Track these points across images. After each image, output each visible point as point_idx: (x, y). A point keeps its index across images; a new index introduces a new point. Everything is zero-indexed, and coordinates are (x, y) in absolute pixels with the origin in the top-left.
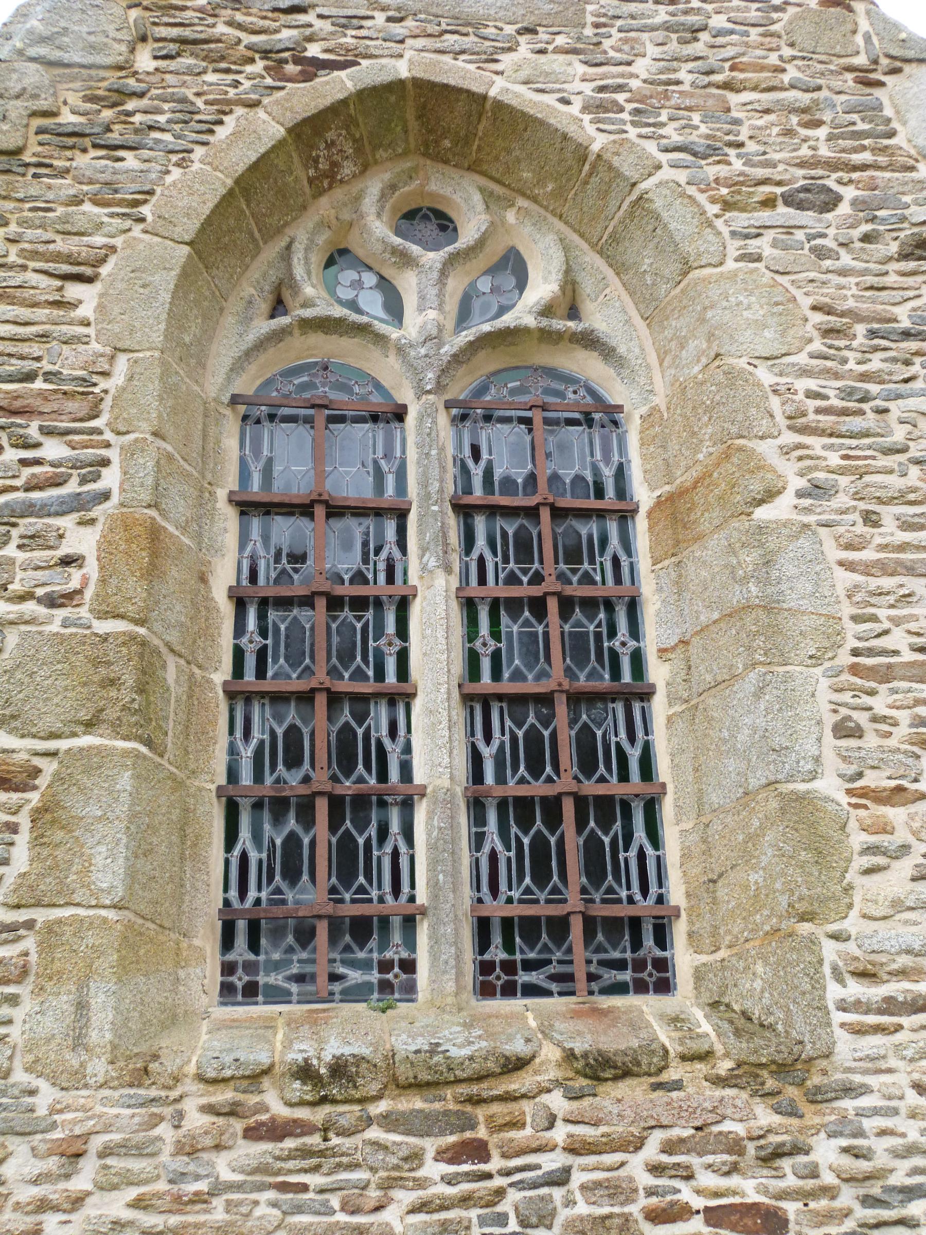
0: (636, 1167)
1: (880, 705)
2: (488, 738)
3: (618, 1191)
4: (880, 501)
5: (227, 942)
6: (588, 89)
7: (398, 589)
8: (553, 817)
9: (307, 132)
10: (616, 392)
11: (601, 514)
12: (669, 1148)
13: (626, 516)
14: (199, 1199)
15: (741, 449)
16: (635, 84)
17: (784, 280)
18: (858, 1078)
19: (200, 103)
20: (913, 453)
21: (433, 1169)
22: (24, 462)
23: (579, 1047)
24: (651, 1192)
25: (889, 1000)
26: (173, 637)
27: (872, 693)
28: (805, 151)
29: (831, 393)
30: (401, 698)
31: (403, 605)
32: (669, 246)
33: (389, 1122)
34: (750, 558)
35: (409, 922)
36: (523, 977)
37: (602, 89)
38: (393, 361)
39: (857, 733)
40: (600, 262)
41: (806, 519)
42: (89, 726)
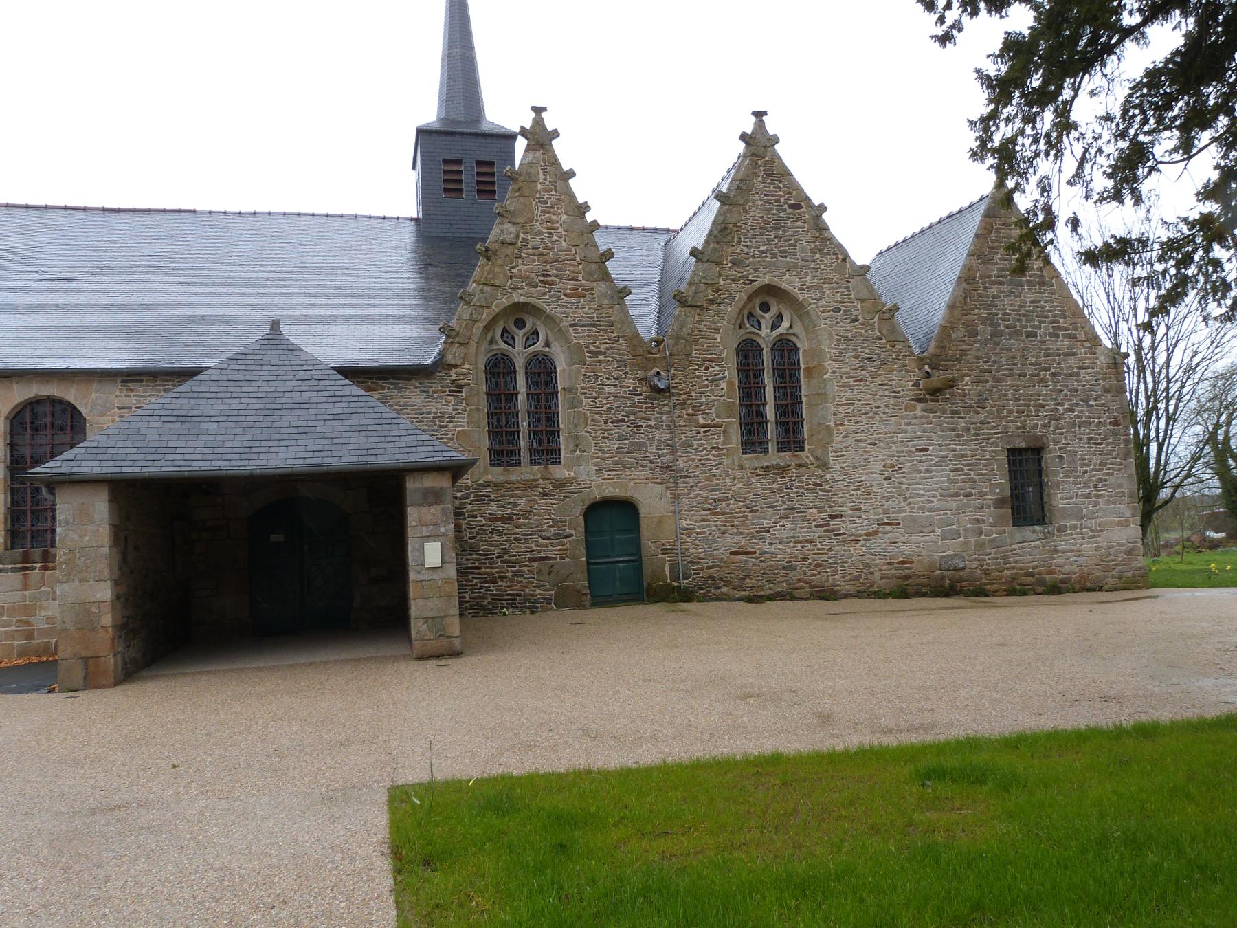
10: (799, 345)
32: (811, 321)
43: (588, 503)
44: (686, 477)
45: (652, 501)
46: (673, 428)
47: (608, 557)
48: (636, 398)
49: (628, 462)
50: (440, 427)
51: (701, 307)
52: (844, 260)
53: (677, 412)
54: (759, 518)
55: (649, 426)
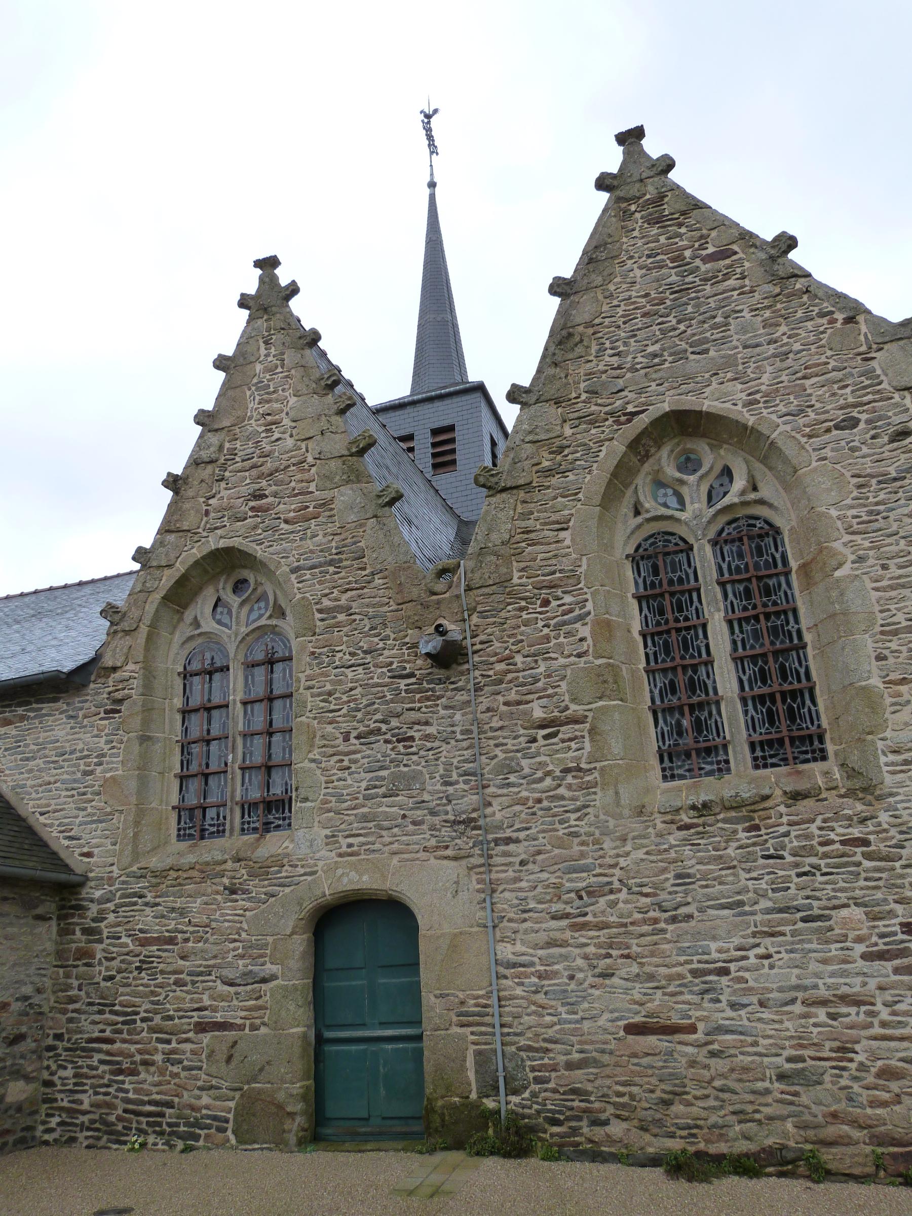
0: (813, 828)
1: (894, 646)
2: (744, 673)
3: (809, 837)
4: (888, 559)
5: (662, 761)
6: (743, 396)
7: (701, 621)
8: (774, 702)
9: (634, 445)
10: (778, 522)
11: (777, 575)
12: (825, 821)
13: (787, 574)
14: (665, 850)
15: (826, 548)
16: (763, 388)
17: (838, 466)
18: (895, 790)
19: (591, 444)
20: (901, 534)
21: (742, 835)
22: (559, 606)
23: (788, 789)
24: (819, 836)
25: (905, 760)
26: (622, 659)
27: (890, 641)
28: (842, 402)
29: (863, 514)
30: (709, 663)
31: (704, 626)
32: (786, 461)
33: (725, 821)
34: (834, 594)
35: (725, 747)
36: (770, 761)
37: (749, 395)
38: (684, 528)
39: (885, 658)
40: (762, 466)
41: (856, 573)
42: (600, 698)
43: (309, 905)
44: (508, 841)
45: (438, 892)
46: (476, 733)
47: (363, 1025)
48: (402, 683)
49: (387, 816)
50: (86, 773)
51: (527, 486)
52: (850, 320)
53: (485, 702)
54: (697, 935)
55: (427, 737)
